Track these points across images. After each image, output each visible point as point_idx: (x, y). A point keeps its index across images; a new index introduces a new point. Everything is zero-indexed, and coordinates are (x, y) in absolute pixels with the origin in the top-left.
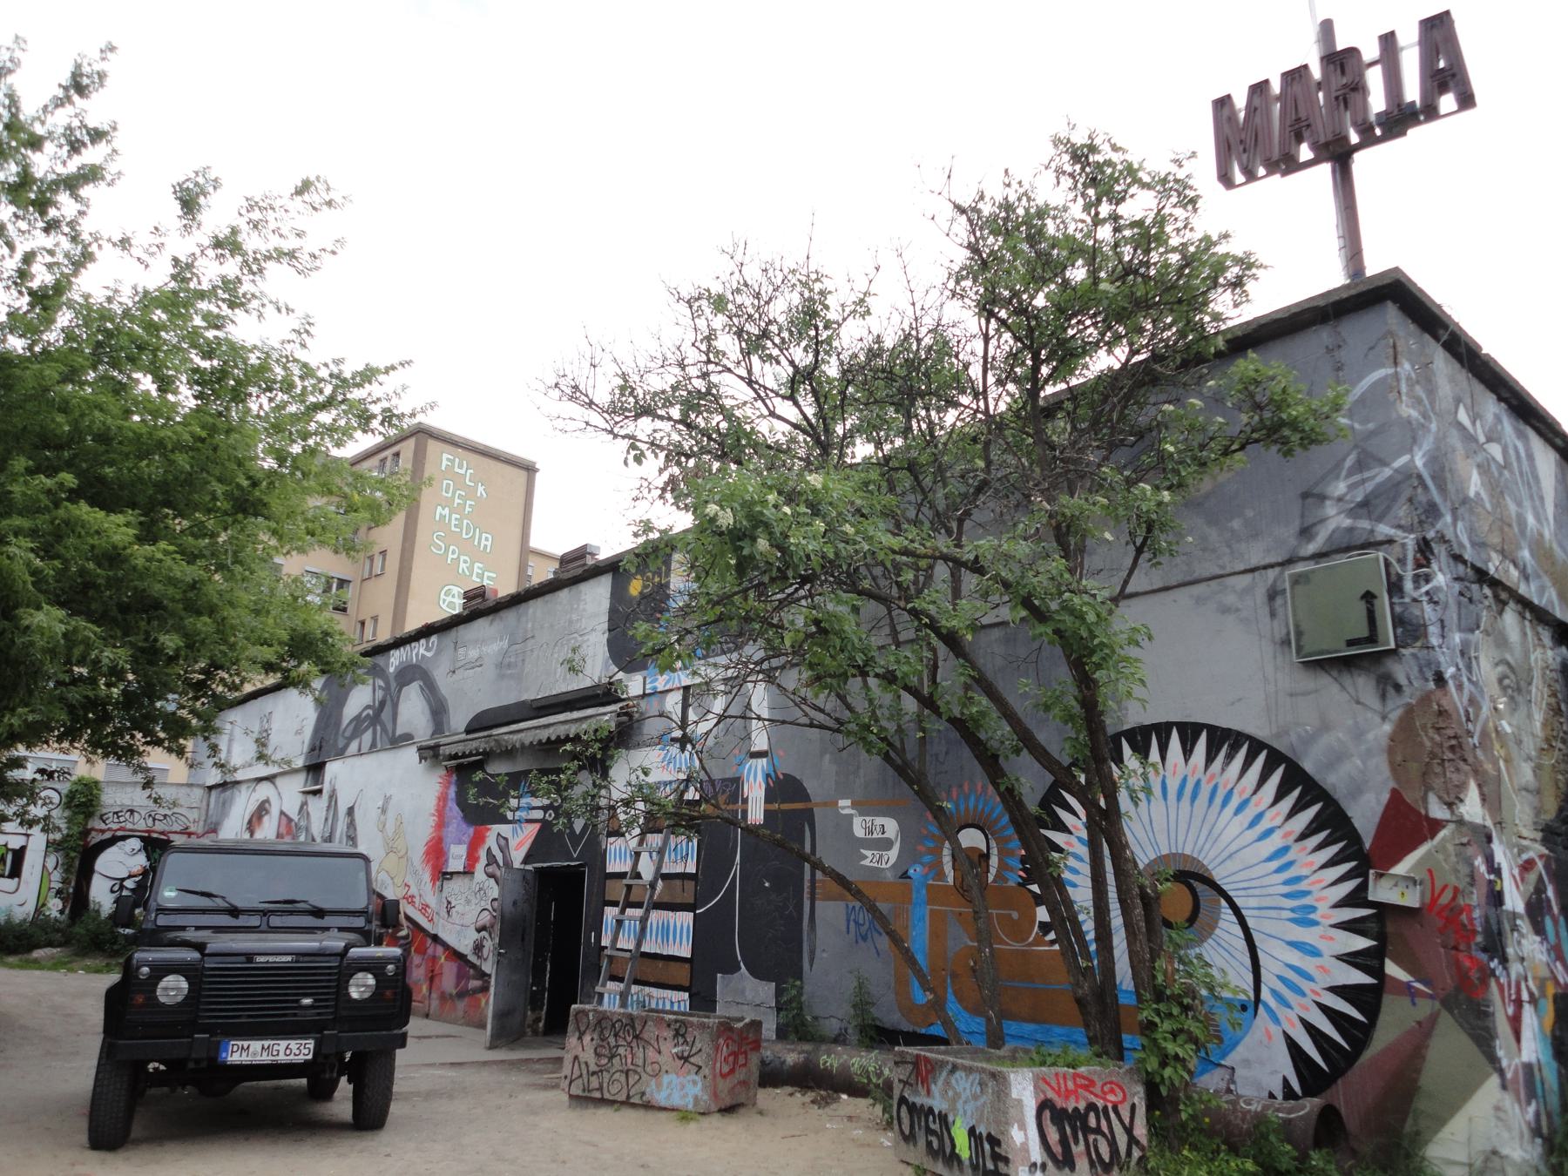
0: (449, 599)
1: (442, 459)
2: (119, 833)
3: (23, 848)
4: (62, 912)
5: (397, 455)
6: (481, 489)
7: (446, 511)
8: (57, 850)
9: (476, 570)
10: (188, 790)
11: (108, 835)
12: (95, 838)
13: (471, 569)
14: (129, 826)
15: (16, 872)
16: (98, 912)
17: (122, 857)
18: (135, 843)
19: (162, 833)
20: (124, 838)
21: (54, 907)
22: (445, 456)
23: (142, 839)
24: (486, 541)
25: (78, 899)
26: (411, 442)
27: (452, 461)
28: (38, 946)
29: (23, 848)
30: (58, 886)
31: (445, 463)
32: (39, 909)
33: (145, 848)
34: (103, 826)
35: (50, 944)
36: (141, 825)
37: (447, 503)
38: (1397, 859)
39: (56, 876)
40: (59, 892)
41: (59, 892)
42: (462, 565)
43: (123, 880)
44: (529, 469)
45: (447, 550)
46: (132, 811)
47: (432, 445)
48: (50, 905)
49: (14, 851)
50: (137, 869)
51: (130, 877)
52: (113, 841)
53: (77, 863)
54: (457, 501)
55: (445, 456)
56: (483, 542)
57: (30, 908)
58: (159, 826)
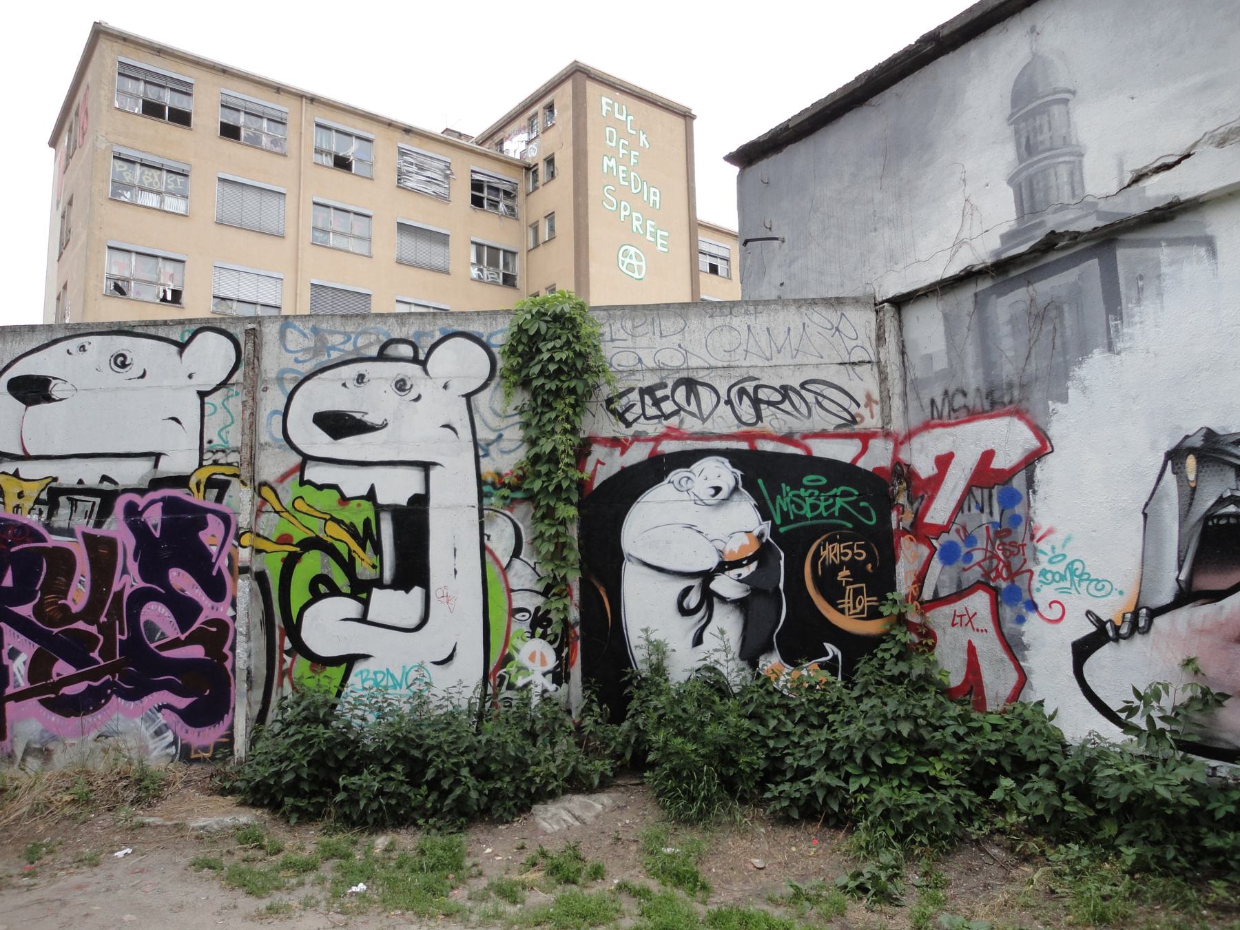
0: (627, 260)
1: (602, 102)
2: (668, 447)
3: (420, 502)
4: (559, 676)
5: (550, 108)
6: (643, 137)
7: (613, 163)
8: (510, 503)
9: (649, 228)
10: (833, 315)
11: (638, 454)
12: (606, 465)
13: (644, 227)
14: (691, 424)
15: (413, 571)
16: (658, 669)
17: (693, 514)
18: (719, 472)
19: (787, 439)
20: (686, 459)
21: (535, 658)
22: (604, 100)
23: (735, 458)
24: (655, 198)
25: (597, 641)
26: (568, 86)
27: (612, 106)
28: (546, 795)
29: (420, 502)
30: (532, 602)
31: (605, 108)
32: (496, 669)
33: (749, 484)
34: (622, 431)
35: (577, 784)
36: (723, 421)
37: (613, 153)
38: (580, 528)
39: (522, 575)
40: (539, 621)
41: (539, 621)
42: (636, 223)
43: (707, 576)
44: (687, 116)
45: (618, 207)
46: (691, 384)
47: (592, 88)
48: (522, 657)
49: (395, 511)
50: (739, 545)
51: (723, 567)
52: (656, 469)
53: (574, 531)
54: (622, 151)
55: (604, 100)
56: (652, 198)
57: (468, 671)
58: (774, 421)
